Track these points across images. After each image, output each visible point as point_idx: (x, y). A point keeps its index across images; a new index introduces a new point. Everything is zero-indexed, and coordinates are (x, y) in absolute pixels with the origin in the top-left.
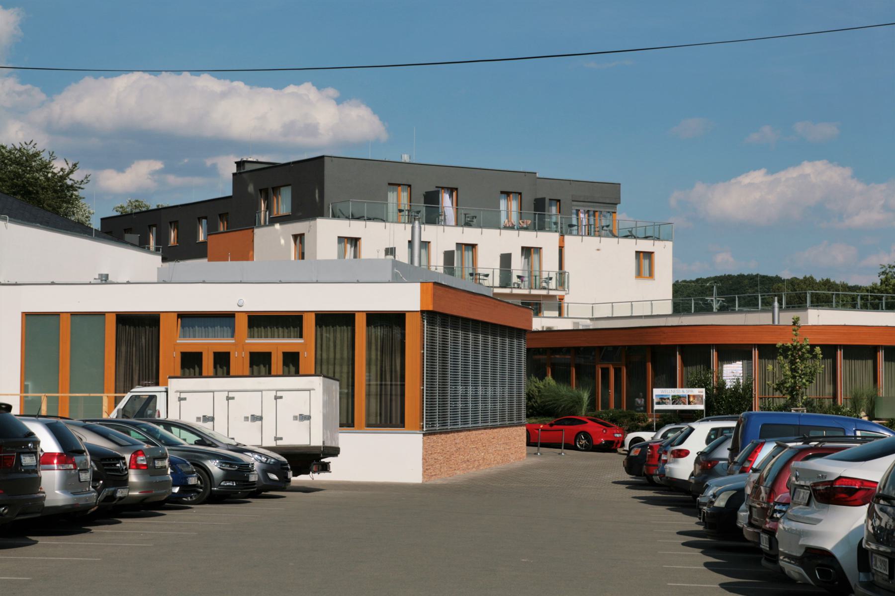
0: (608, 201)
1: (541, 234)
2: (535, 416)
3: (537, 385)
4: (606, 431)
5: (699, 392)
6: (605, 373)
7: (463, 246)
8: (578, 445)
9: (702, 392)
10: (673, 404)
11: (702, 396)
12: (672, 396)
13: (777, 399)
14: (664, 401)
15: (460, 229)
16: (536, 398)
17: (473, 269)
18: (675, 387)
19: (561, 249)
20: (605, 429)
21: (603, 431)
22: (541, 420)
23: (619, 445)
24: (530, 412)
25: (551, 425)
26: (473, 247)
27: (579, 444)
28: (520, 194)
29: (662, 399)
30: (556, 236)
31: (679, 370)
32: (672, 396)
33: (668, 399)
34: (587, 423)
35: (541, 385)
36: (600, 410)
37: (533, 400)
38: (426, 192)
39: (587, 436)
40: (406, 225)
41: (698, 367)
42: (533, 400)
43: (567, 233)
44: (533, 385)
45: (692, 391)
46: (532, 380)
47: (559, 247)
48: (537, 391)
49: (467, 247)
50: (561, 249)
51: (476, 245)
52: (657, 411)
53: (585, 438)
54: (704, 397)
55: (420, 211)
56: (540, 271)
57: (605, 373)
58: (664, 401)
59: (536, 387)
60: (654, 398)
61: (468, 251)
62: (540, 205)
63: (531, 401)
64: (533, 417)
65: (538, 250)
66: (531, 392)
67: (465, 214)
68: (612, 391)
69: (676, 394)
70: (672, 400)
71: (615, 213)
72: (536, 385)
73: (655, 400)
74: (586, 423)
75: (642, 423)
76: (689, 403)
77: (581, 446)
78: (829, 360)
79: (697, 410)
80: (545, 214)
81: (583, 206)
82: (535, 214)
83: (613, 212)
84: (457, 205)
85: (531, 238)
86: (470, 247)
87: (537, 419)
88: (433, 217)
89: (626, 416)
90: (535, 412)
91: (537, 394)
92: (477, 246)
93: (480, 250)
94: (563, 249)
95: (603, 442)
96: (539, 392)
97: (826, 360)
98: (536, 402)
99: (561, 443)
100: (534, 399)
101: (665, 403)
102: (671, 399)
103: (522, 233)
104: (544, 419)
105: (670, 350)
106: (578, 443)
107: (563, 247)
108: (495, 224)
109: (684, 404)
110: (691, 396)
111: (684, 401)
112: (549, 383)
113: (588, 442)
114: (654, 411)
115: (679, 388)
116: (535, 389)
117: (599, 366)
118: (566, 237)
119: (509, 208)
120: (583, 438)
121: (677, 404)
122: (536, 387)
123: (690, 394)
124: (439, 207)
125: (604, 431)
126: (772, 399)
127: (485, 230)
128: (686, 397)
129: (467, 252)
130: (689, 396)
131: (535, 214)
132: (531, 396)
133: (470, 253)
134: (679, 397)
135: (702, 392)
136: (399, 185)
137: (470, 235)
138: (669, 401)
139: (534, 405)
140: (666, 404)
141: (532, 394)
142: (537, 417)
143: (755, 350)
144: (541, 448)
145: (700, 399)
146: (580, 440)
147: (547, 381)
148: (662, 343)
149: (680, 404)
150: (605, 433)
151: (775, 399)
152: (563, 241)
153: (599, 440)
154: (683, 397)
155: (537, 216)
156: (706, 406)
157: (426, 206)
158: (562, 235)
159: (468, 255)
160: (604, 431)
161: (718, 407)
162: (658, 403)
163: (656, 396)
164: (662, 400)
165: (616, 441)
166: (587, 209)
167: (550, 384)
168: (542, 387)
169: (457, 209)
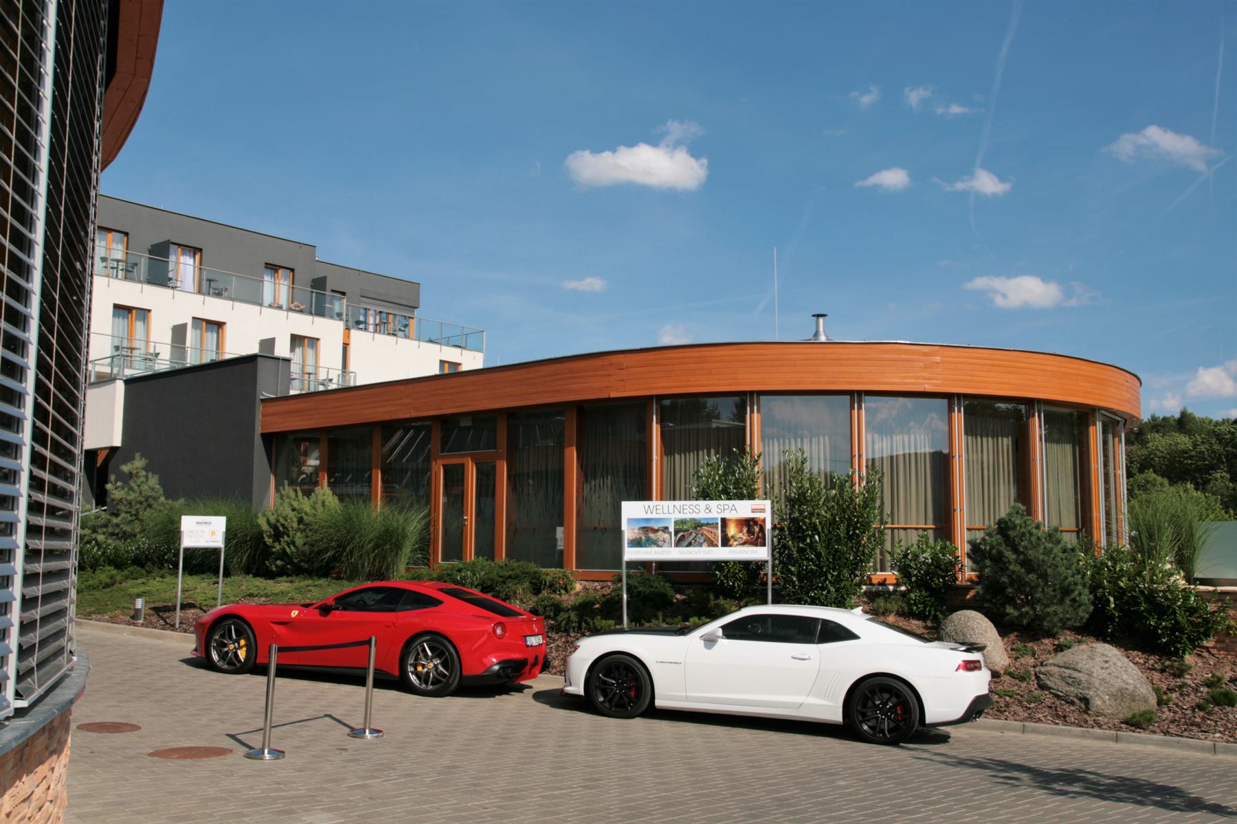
0: (404, 303)
1: (319, 320)
2: (288, 575)
3: (296, 506)
4: (504, 630)
5: (754, 511)
6: (454, 478)
7: (204, 323)
8: (413, 678)
9: (763, 511)
10: (678, 544)
11: (764, 520)
12: (676, 523)
13: (901, 531)
14: (652, 535)
15: (201, 297)
16: (291, 533)
17: (217, 353)
18: (648, 497)
19: (346, 346)
20: (498, 624)
21: (494, 631)
22: (302, 584)
23: (540, 666)
24: (277, 566)
25: (325, 610)
26: (219, 325)
27: (418, 675)
28: (292, 270)
29: (646, 530)
30: (339, 326)
31: (657, 460)
32: (676, 523)
33: (666, 529)
34: (441, 602)
35: (305, 504)
36: (440, 561)
37: (286, 538)
38: (152, 246)
39: (440, 643)
40: (111, 280)
41: (703, 456)
42: (286, 538)
43: (353, 328)
44: (286, 505)
45: (734, 509)
46: (283, 492)
47: (344, 344)
48: (295, 519)
49: (210, 325)
50: (346, 346)
51: (224, 323)
52: (632, 564)
53: (438, 653)
54: (768, 526)
55: (136, 264)
56: (317, 367)
57: (454, 478)
58: (652, 535)
59: (294, 510)
60: (624, 526)
61: (212, 332)
62: (319, 284)
63: (279, 541)
64: (284, 578)
65: (314, 341)
66: (282, 520)
67: (210, 281)
68: (470, 518)
69: (687, 516)
70: (676, 532)
71: (413, 318)
72: (295, 504)
73: (628, 532)
74: (435, 602)
75: (560, 595)
76: (726, 542)
77: (424, 678)
78: (1005, 439)
79: (726, 562)
80: (324, 294)
81: (374, 304)
82: (312, 292)
83: (410, 317)
84: (201, 264)
85: (306, 325)
86: (215, 327)
87: (291, 582)
88: (160, 277)
89: (517, 577)
90: (289, 566)
91: (295, 525)
92: (225, 326)
93: (229, 330)
94: (348, 347)
95: (496, 668)
96: (300, 521)
97: (1000, 439)
98: (293, 543)
99: (366, 669)
100: (289, 536)
101: (655, 543)
102: (672, 529)
103: (291, 314)
104: (310, 582)
105: (638, 407)
106: (410, 669)
107: (348, 344)
108: (256, 299)
109: (712, 544)
110: (729, 520)
111: (709, 535)
112: (323, 502)
113: (445, 665)
114: (624, 565)
115: (657, 500)
116: (292, 514)
117: (440, 462)
118: (354, 332)
119: (276, 288)
120: (429, 653)
121: (689, 545)
122: (294, 510)
123: (727, 515)
124: (168, 262)
125: (499, 631)
126: (890, 531)
127: (237, 304)
128: (715, 525)
129: (209, 334)
130: (724, 521)
131: (312, 292)
132: (281, 529)
133: (215, 335)
134: (698, 525)
135: (763, 511)
136: (110, 230)
137: (214, 308)
138: (666, 536)
139: (288, 550)
140: (658, 546)
141: (283, 525)
142: (294, 578)
143: (752, 411)
144: (280, 682)
145: (757, 529)
146: (417, 659)
147: (321, 498)
148: (614, 394)
149: (701, 545)
150: (500, 637)
151: (896, 531)
152: (349, 336)
153: (486, 661)
154: (707, 524)
155: (314, 295)
156: (779, 550)
157: (150, 258)
158: (348, 329)
159: (211, 337)
160: (499, 631)
161: (801, 551)
162: (636, 543)
163: (630, 520)
164: (648, 534)
165: (531, 660)
166: (379, 310)
167: (326, 503)
168: (307, 509)
169: (200, 269)
